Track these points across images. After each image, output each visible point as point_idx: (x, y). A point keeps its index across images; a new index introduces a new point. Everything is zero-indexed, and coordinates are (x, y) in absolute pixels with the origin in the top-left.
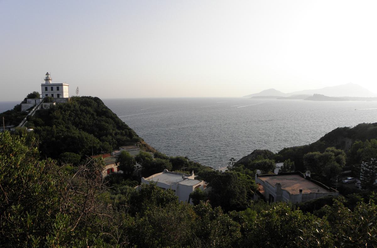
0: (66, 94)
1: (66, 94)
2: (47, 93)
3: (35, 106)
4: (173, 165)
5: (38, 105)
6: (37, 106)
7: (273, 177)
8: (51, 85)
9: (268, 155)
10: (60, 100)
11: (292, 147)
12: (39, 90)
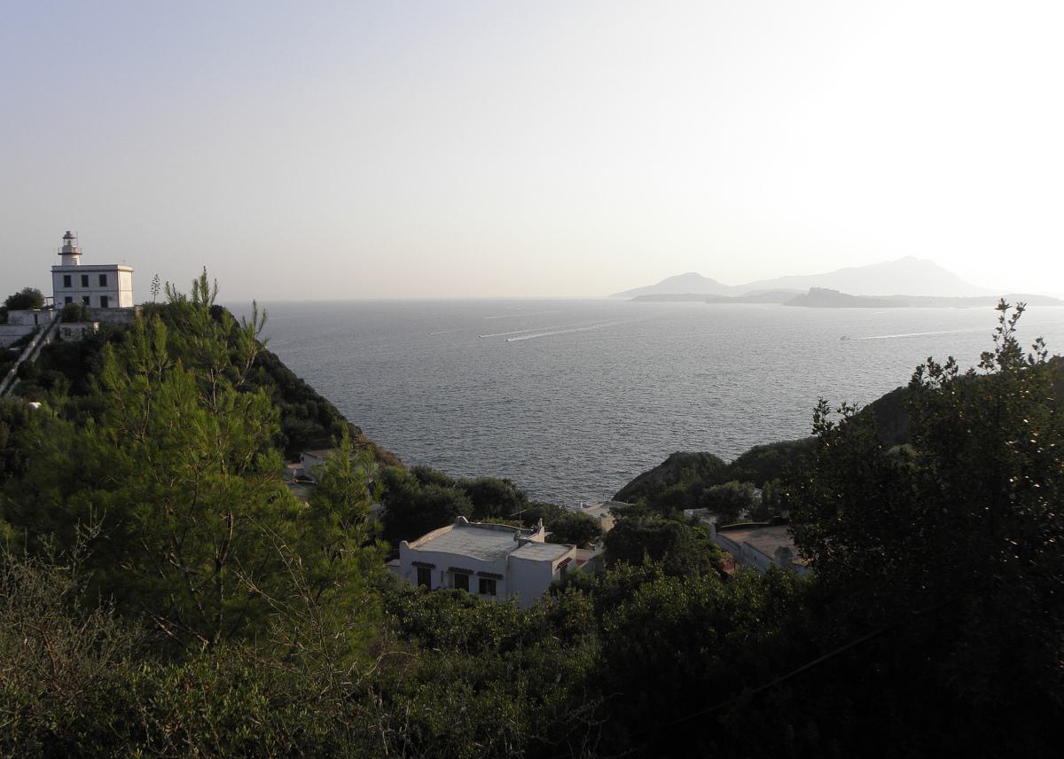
0: (126, 299)
1: (126, 299)
2: (68, 295)
3: (36, 331)
4: (476, 502)
5: (46, 328)
6: (42, 332)
7: (759, 531)
8: (84, 271)
9: (709, 468)
10: (109, 313)
11: (775, 442)
12: (46, 288)
